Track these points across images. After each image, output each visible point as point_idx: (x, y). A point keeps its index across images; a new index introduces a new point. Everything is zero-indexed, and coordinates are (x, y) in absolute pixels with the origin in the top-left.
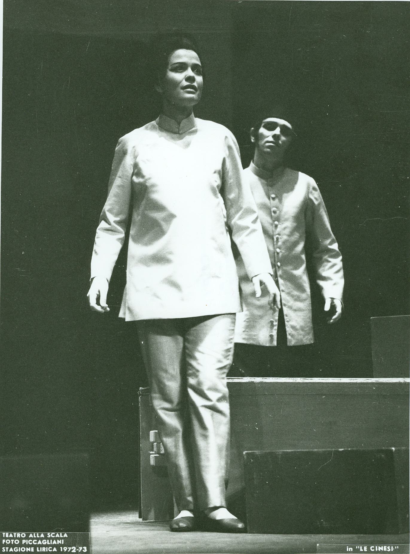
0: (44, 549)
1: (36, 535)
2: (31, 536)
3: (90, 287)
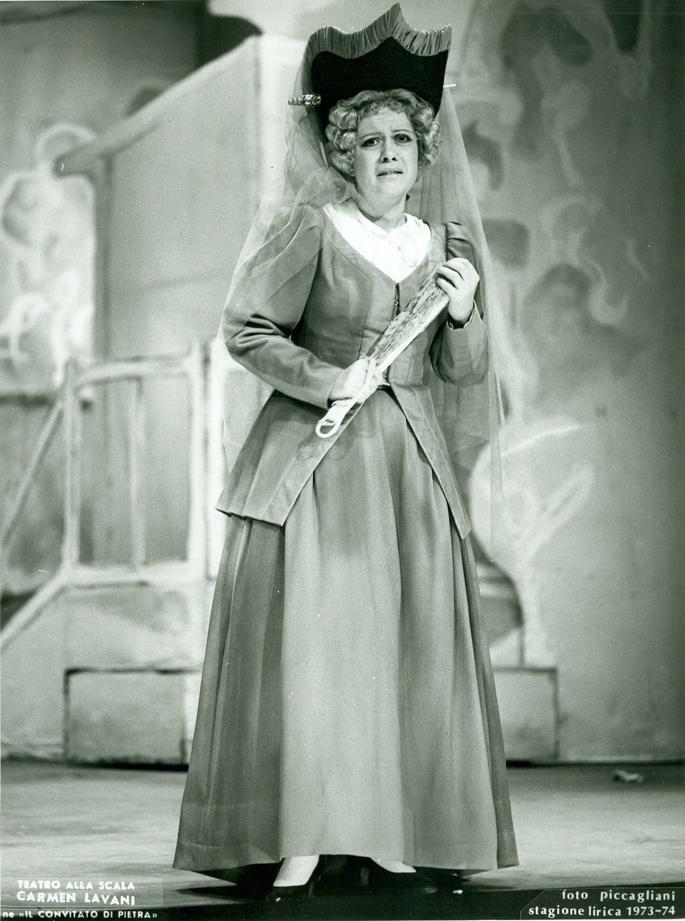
1: (78, 885)
2: (69, 886)
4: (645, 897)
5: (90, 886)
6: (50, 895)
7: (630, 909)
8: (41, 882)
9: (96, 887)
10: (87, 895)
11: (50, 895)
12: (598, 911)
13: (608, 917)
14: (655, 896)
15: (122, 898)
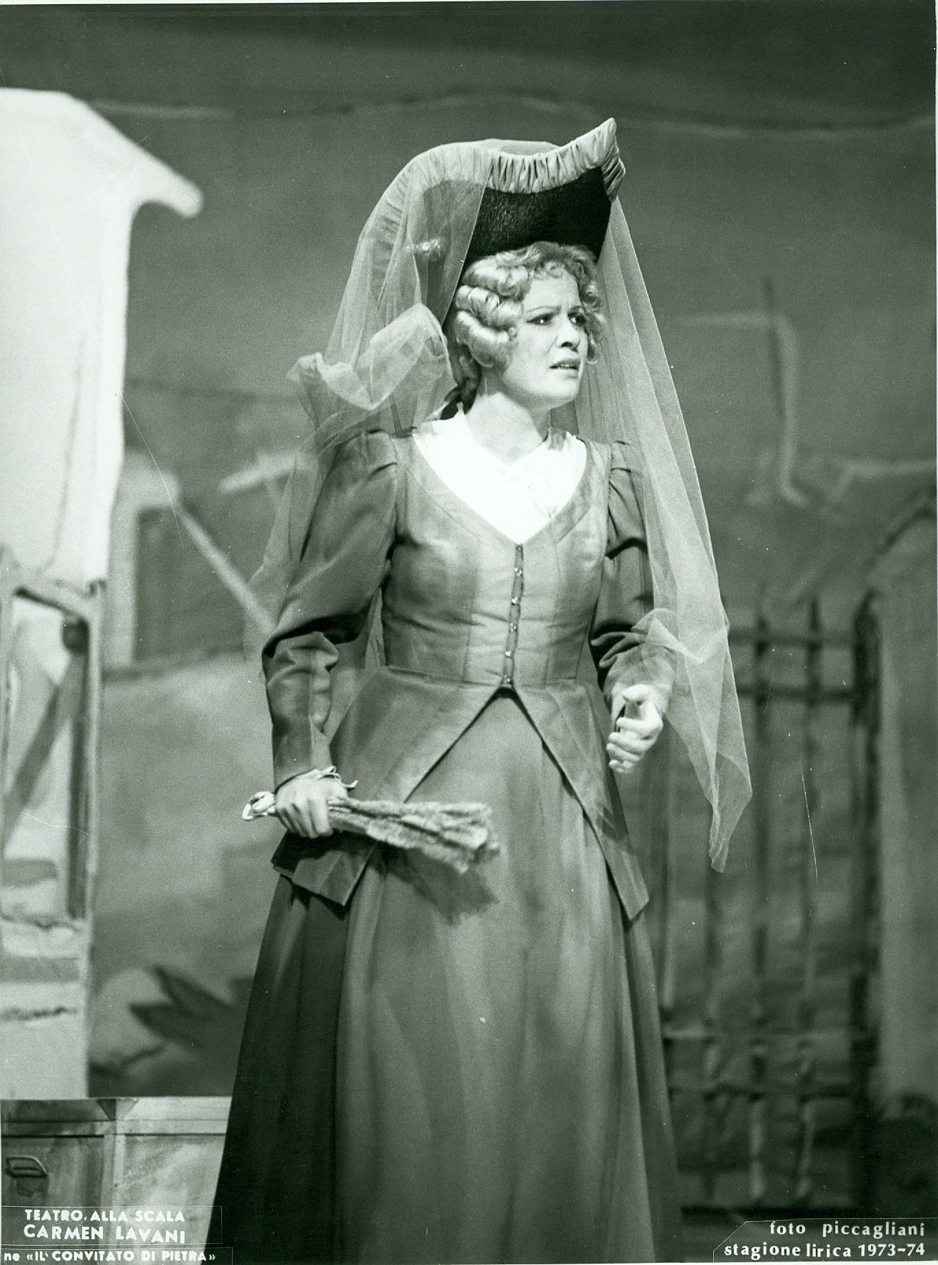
1: (108, 1216)
2: (95, 1217)
7: (863, 1247)
12: (820, 1250)
13: (833, 1259)
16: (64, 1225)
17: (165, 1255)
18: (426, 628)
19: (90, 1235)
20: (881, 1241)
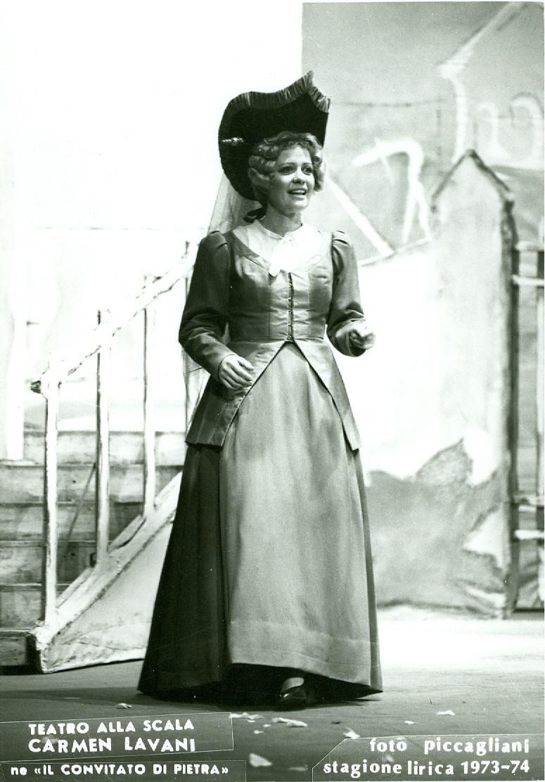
0: (77, 769)
1: (115, 727)
2: (102, 728)
3: (220, 128)
4: (487, 747)
5: (131, 727)
6: (75, 743)
8: (61, 726)
9: (139, 727)
10: (127, 740)
11: (75, 743)
12: (422, 768)
13: (435, 777)
14: (501, 746)
15: (178, 743)
16: (70, 739)
17: (158, 769)
18: (250, 317)
19: (97, 747)
20: (484, 758)
